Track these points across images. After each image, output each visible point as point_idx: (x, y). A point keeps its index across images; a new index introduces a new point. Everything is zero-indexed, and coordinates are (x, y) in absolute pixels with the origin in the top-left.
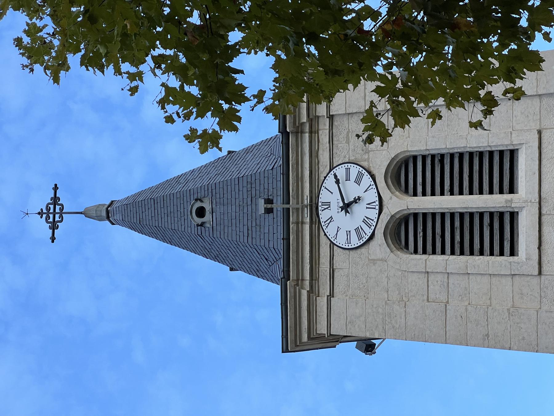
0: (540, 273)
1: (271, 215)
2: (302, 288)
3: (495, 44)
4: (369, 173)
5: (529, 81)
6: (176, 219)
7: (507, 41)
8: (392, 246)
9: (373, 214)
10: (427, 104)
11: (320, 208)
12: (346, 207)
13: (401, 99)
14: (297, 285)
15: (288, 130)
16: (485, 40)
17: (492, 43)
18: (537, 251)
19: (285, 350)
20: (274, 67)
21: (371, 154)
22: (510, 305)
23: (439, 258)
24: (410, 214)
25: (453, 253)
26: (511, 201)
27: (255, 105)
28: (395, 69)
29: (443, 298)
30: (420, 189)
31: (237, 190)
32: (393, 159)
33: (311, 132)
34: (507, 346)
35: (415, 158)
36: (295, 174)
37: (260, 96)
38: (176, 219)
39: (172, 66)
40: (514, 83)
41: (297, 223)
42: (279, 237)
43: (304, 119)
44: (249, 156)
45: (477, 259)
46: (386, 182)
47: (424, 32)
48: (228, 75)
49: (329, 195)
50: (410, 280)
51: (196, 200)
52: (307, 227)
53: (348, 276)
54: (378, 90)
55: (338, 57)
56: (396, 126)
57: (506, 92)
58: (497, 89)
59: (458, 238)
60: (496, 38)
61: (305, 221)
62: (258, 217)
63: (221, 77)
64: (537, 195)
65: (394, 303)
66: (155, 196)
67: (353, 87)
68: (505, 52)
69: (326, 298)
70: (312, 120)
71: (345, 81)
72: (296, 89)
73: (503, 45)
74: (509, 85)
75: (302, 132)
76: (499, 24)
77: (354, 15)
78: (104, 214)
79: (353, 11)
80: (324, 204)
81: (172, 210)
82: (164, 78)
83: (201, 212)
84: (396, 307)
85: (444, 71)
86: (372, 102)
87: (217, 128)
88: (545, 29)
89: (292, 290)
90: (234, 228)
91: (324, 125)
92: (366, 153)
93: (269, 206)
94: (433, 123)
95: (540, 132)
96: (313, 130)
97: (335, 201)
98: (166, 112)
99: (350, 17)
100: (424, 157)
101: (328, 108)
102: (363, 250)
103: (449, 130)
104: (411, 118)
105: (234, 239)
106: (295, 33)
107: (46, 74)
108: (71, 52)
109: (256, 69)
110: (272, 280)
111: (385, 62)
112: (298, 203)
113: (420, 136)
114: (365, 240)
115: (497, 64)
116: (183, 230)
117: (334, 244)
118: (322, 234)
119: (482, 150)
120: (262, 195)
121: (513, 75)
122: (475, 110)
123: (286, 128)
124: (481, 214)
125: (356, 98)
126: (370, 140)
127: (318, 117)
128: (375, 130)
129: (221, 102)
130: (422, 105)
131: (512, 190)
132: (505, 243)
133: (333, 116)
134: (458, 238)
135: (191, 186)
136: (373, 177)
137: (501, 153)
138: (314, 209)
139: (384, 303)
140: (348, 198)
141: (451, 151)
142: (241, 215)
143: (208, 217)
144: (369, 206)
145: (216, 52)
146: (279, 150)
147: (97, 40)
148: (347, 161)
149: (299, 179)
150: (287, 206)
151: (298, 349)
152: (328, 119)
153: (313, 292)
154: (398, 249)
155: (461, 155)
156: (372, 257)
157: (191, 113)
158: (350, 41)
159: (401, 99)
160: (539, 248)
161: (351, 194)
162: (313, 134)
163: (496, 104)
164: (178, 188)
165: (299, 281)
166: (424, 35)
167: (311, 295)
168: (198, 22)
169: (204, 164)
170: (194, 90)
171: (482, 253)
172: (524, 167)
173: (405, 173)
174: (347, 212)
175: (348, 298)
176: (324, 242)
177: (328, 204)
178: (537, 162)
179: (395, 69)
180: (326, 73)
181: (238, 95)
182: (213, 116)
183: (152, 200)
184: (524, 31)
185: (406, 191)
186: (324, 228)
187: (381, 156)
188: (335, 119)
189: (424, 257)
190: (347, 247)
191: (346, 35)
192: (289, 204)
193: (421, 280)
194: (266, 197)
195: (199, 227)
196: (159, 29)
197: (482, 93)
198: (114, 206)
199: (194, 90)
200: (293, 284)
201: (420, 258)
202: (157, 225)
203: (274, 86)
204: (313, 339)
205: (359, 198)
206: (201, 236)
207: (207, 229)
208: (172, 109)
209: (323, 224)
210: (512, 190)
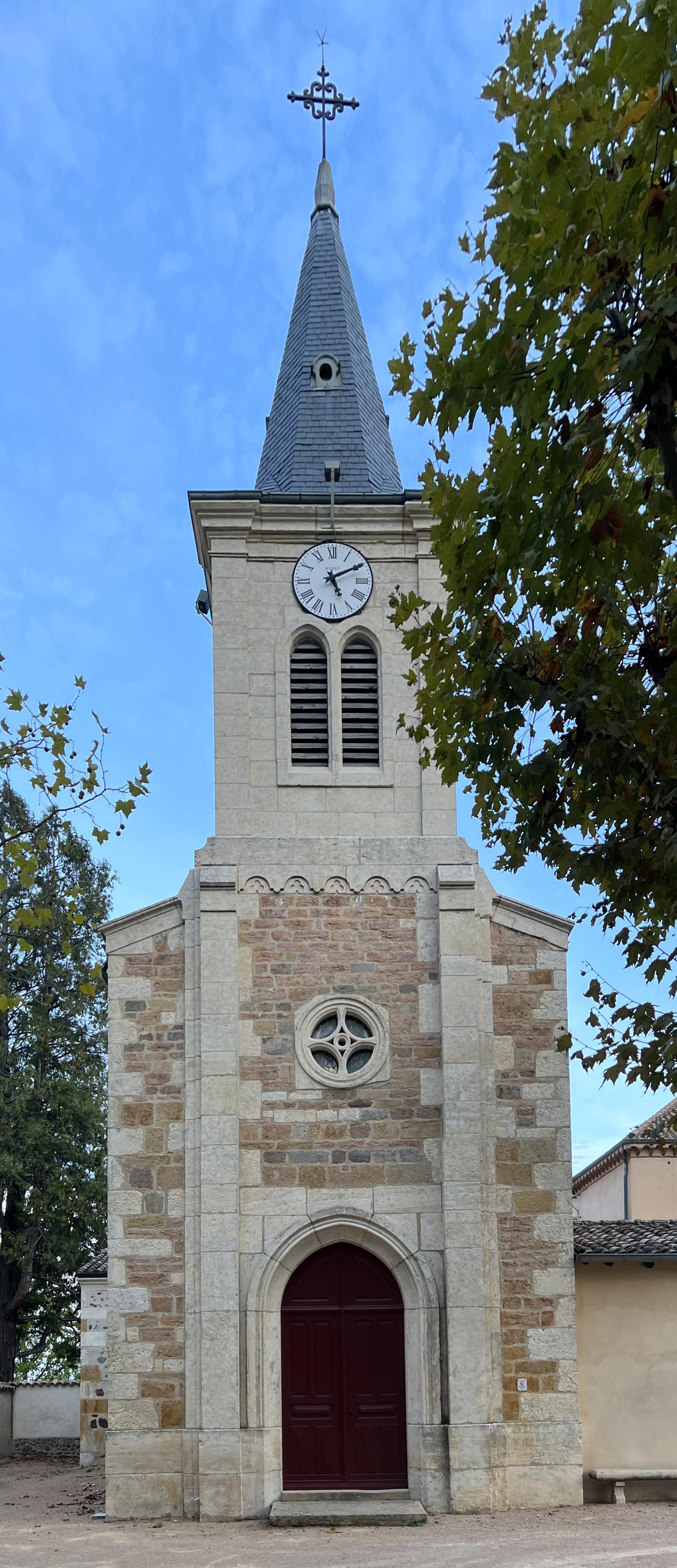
0: (279, 786)
1: (323, 478)
2: (254, 521)
3: (467, 740)
4: (363, 608)
5: (434, 772)
6: (318, 331)
7: (468, 751)
8: (297, 634)
9: (325, 613)
10: (421, 670)
11: (330, 544)
13: (429, 640)
14: (256, 514)
15: (407, 503)
16: (471, 730)
17: (468, 736)
18: (297, 784)
19: (193, 496)
20: (472, 475)
21: (379, 610)
22: (253, 758)
23: (288, 687)
24: (325, 655)
25: (293, 701)
26: (337, 760)
27: (434, 447)
28: (456, 631)
29: (254, 691)
30: (348, 666)
31: (349, 429)
32: (375, 636)
33: (403, 534)
34: (218, 755)
35: (374, 661)
36: (364, 512)
37: (443, 455)
38: (318, 331)
39: (486, 315)
40: (434, 759)
41: (316, 515)
42: (303, 489)
43: (418, 525)
44: (382, 447)
45: (288, 726)
46: (355, 628)
47: (486, 664)
48: (469, 405)
49: (344, 557)
50: (267, 654)
51: (339, 365)
52: (311, 527)
53: (268, 580)
54: (439, 611)
55: (473, 561)
56: (405, 633)
57: (427, 751)
58: (430, 743)
59: (306, 706)
60: (472, 740)
61: (319, 524)
62: (322, 460)
63: (468, 394)
64: (341, 784)
65: (246, 636)
66: (344, 295)
67: (443, 581)
68: (460, 750)
69: (245, 551)
70: (415, 535)
71: (450, 571)
72: (448, 496)
73: (465, 747)
74: (432, 753)
75: (403, 522)
76: (483, 743)
77: (510, 583)
78: (324, 201)
79: (515, 582)
80: (335, 549)
81: (328, 325)
82: (473, 301)
83: (326, 372)
84: (242, 638)
85: (449, 687)
86: (429, 603)
87: (414, 389)
88: (474, 787)
89: (250, 507)
90: (310, 424)
92: (381, 604)
93: (333, 476)
94: (405, 676)
95: (391, 787)
96: (406, 537)
97: (338, 565)
98: (436, 304)
99: (509, 578)
100: (374, 671)
101: (425, 557)
102: (293, 599)
103: (399, 696)
104: (410, 651)
105: (299, 424)
106: (502, 504)
107: (495, 72)
108: (518, 123)
109: (471, 449)
110: (260, 481)
111: (464, 620)
112: (336, 515)
113: (396, 664)
114: (301, 601)
115: (450, 742)
116: (307, 343)
117: (297, 562)
118: (307, 547)
119: (380, 731)
120: (344, 466)
121: (440, 757)
122: (414, 718)
123: (409, 499)
124: (325, 731)
125: (432, 584)
126: (393, 603)
127: (417, 544)
128: (405, 606)
129: (442, 393)
130: (422, 665)
131: (346, 761)
132: (302, 754)
133: (417, 562)
134: (306, 706)
135: (354, 356)
136: (359, 612)
137: (376, 751)
138: (329, 537)
139: (245, 624)
140: (340, 580)
141: (379, 701)
142: (323, 435)
143: (321, 383)
144: (333, 608)
145: (494, 387)
146: (387, 490)
147: (527, 177)
148: (375, 580)
149: (358, 517)
150: (332, 502)
151: (194, 513)
152: (414, 556)
154: (294, 641)
155: (375, 711)
156: (286, 611)
157: (432, 346)
158: (486, 578)
159: (429, 640)
160: (299, 786)
161: (346, 584)
162: (400, 537)
163: (418, 740)
164: (352, 336)
165: (260, 517)
166: (483, 665)
167: (247, 532)
168: (528, 360)
169: (377, 379)
170: (456, 353)
171: (294, 731)
173: (362, 647)
175: (247, 579)
176: (292, 551)
177: (334, 557)
178: (368, 784)
179: (456, 631)
180: (459, 547)
181: (447, 424)
182: (428, 380)
183: (337, 291)
184: (474, 767)
185: (347, 651)
186: (312, 550)
187: (377, 622)
188: (414, 565)
189: (289, 671)
190: (295, 579)
191: (494, 573)
192: (336, 503)
193: (267, 669)
194: (342, 472)
195: (309, 369)
196: (529, 290)
197: (428, 727)
198: (332, 220)
199: (456, 353)
200: (257, 508)
201: (287, 666)
202: (312, 298)
203: (453, 476)
204: (205, 533)
206: (298, 375)
207: (308, 382)
208: (439, 310)
209: (315, 548)
210: (346, 761)
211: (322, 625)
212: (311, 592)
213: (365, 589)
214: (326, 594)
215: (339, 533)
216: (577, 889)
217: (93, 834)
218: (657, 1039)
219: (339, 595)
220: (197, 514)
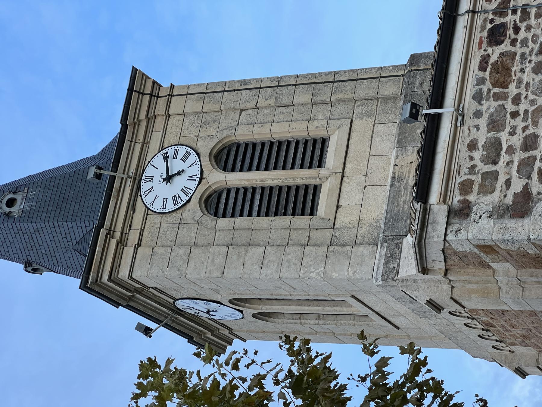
9: (193, 185)
11: (142, 181)
12: (169, 179)
41: (131, 142)
43: (143, 116)
49: (156, 169)
80: (147, 177)
91: (160, 122)
114: (180, 205)
117: (148, 209)
136: (198, 155)
138: (137, 181)
144: (190, 178)
150: (114, 174)
153: (122, 243)
161: (176, 165)
172: (324, 205)
173: (228, 156)
174: (248, 368)
176: (140, 208)
185: (216, 215)
205: (183, 171)
211: (202, 188)
213: (183, 150)
214: (179, 182)
215: (136, 175)
217: (402, 353)
218: (383, 369)
219: (183, 171)
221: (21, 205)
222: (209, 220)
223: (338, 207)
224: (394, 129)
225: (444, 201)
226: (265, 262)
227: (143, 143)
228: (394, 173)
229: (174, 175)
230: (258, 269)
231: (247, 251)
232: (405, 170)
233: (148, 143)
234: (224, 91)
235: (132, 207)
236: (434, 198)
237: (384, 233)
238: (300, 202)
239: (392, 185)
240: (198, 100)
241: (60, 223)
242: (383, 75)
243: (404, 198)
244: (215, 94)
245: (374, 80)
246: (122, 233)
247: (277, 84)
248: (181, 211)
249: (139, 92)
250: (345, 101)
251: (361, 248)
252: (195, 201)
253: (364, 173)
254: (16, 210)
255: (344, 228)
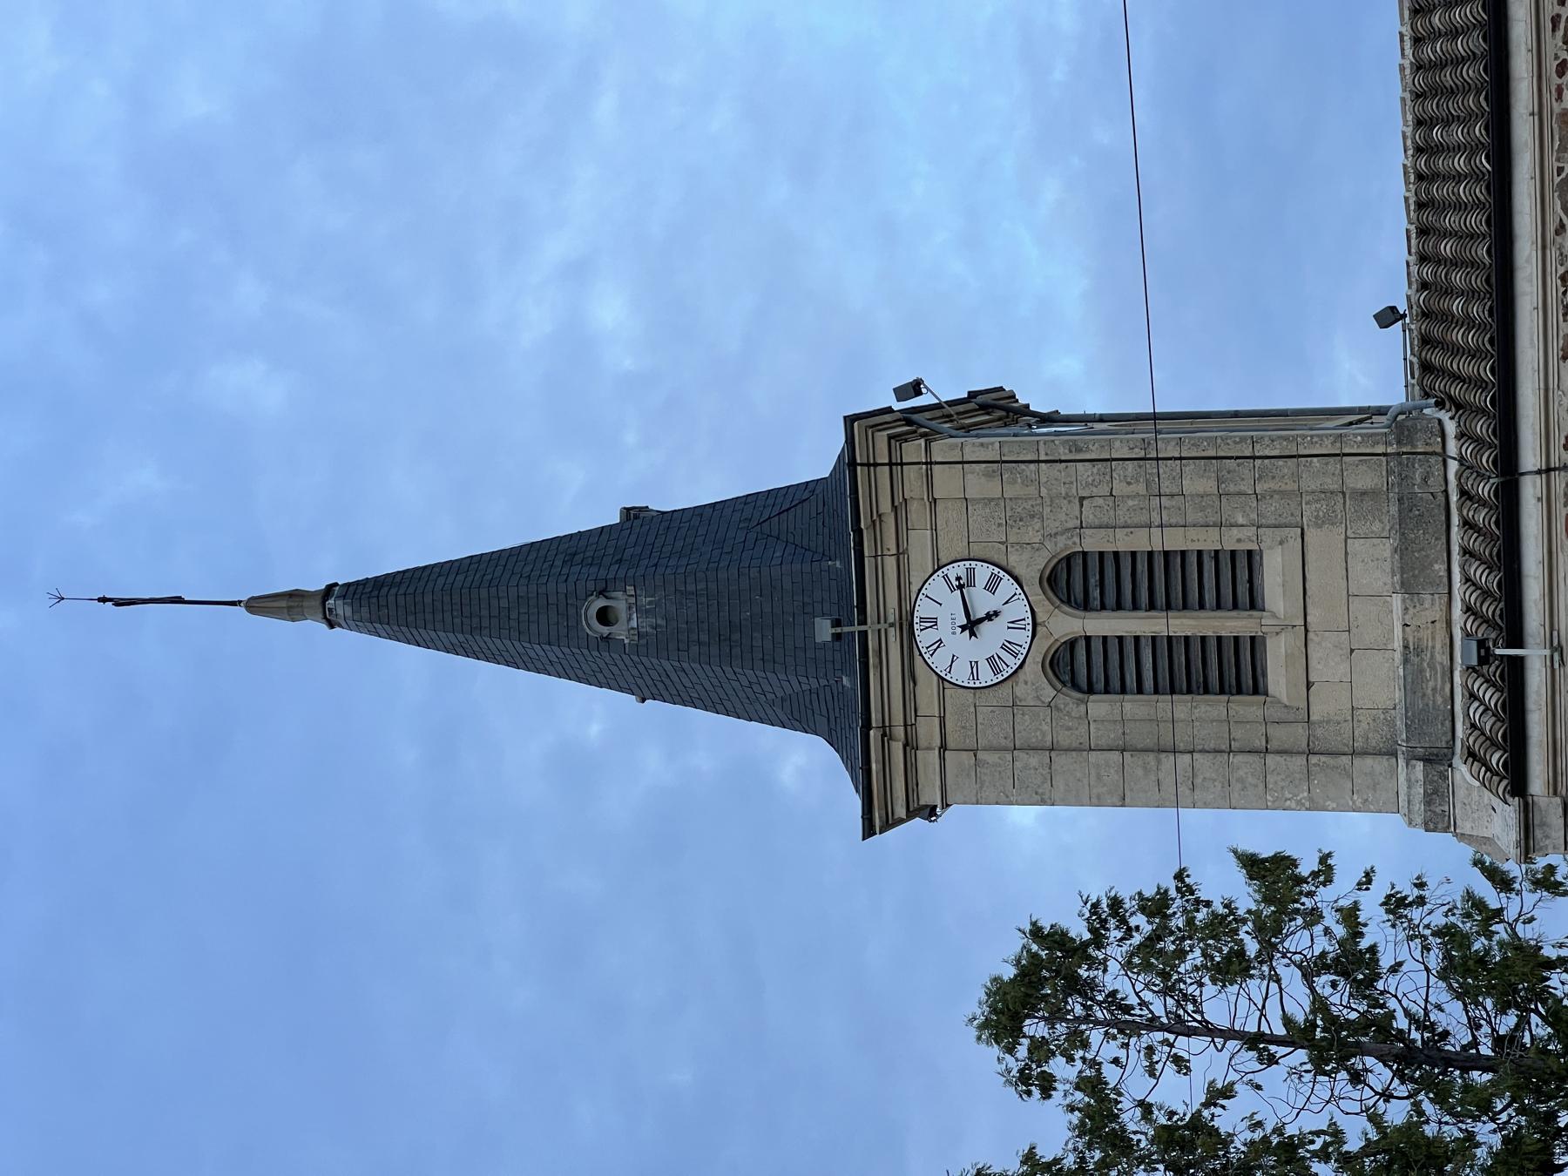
9: (1023, 637)
12: (971, 626)
30: (1130, 648)
43: (886, 506)
49: (938, 604)
91: (917, 513)
118: (918, 659)
136: (1016, 579)
144: (1014, 624)
150: (863, 628)
161: (982, 602)
173: (1071, 580)
174: (972, 634)
177: (934, 622)
205: (996, 614)
211: (1042, 645)
212: (990, 660)
216: (1387, 317)
220: (888, 825)
221: (630, 619)
222: (1069, 700)
223: (1309, 685)
224: (1386, 549)
225: (1555, 793)
226: (1198, 781)
227: (898, 555)
228: (1404, 639)
229: (981, 621)
230: (1188, 792)
231: (1159, 762)
232: (1425, 634)
233: (905, 552)
234: (1039, 462)
235: (910, 675)
236: (1537, 783)
237: (1408, 740)
238: (1234, 671)
239: (1406, 661)
240: (989, 475)
241: (738, 670)
242: (1346, 451)
243: (1431, 684)
244: (1023, 466)
245: (1331, 460)
246: (905, 725)
247: (1142, 454)
248: (1009, 683)
249: (868, 465)
250: (1282, 493)
251: (1369, 761)
252: (1033, 669)
253: (1344, 626)
254: (620, 631)
255: (1328, 722)
